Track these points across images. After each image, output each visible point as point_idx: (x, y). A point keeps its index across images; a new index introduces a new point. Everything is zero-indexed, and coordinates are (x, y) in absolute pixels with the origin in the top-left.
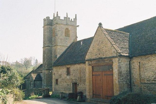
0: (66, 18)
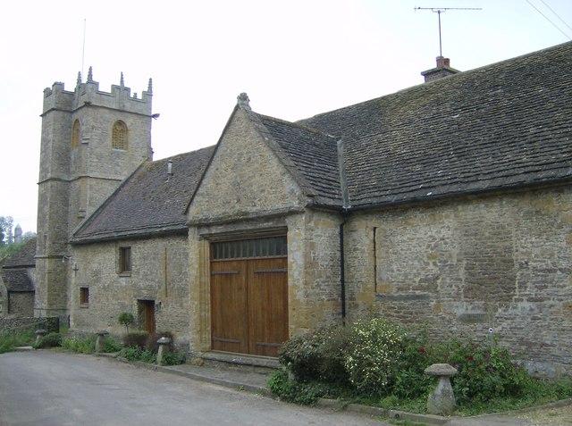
0: (121, 90)
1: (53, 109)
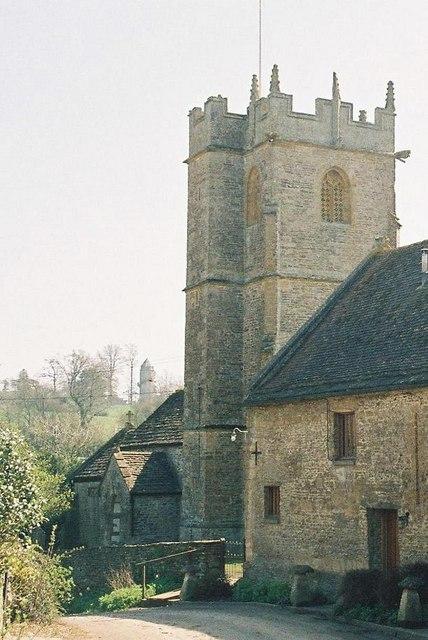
0: (332, 107)
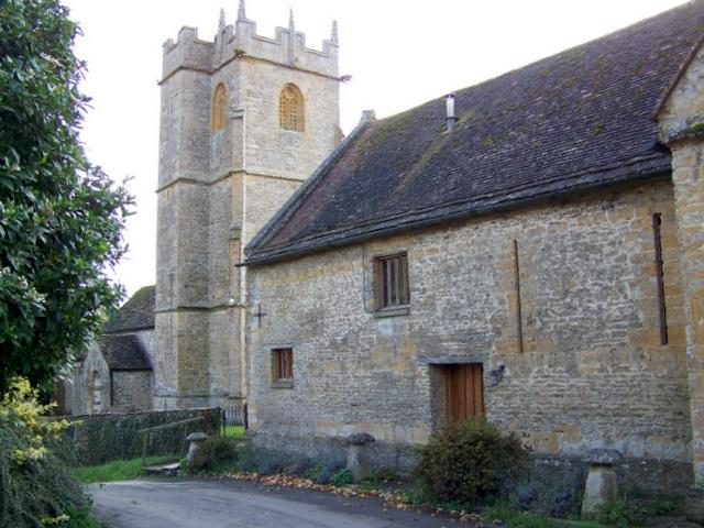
0: (289, 36)
1: (181, 68)
